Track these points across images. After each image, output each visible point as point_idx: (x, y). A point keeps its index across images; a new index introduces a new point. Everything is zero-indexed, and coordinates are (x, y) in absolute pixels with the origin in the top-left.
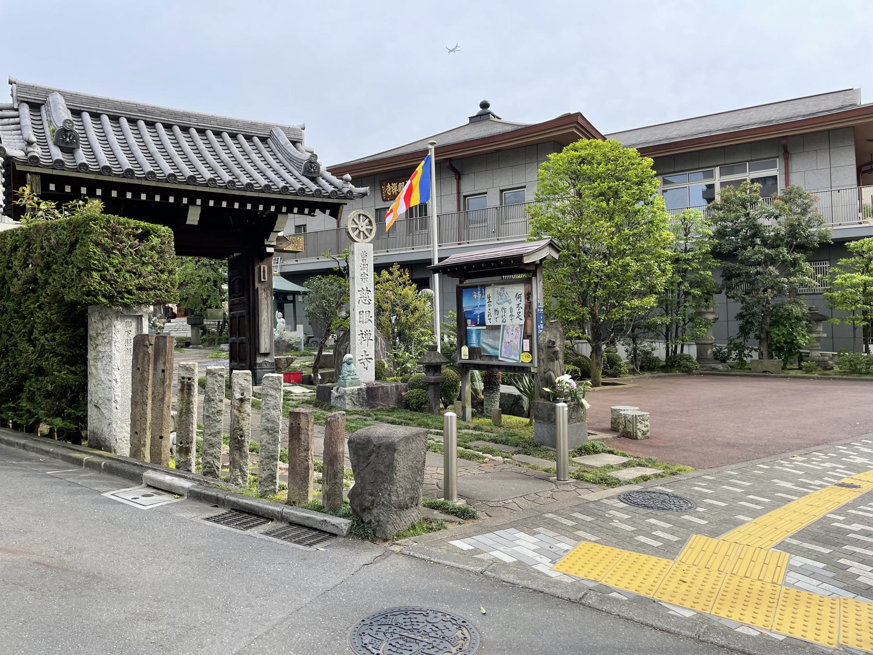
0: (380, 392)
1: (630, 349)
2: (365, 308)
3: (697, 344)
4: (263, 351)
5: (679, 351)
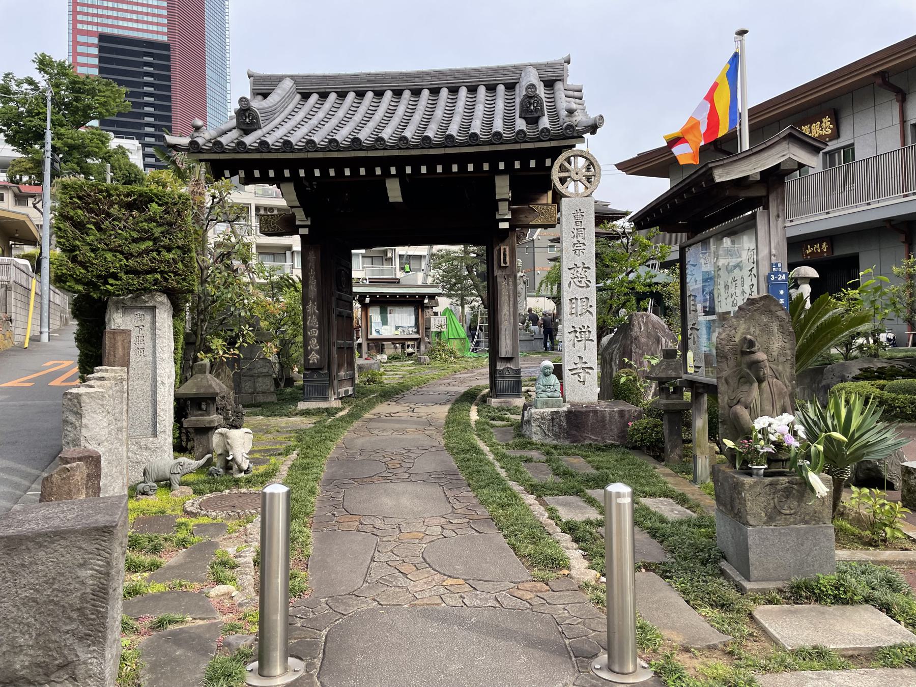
0: (591, 419)
2: (580, 293)
4: (503, 354)
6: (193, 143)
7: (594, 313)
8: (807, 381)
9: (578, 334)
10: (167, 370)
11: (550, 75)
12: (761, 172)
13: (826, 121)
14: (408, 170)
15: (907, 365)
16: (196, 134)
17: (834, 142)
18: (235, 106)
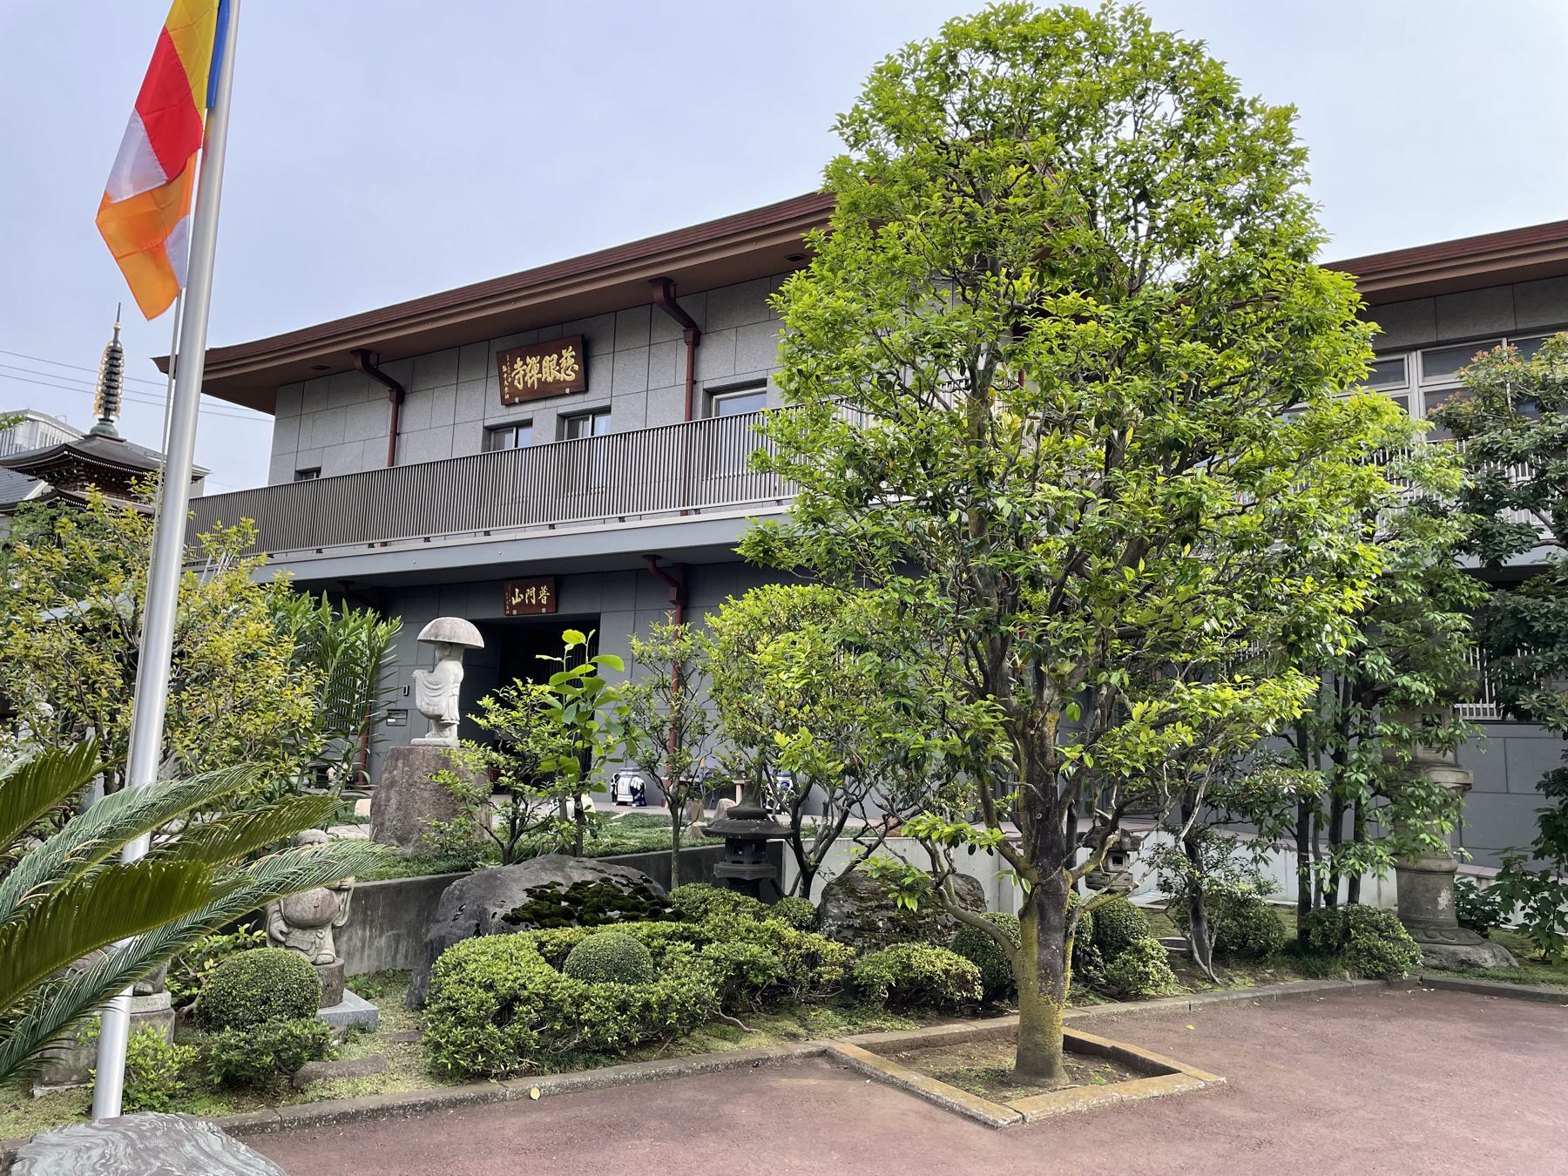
1: (1177, 882)
3: (1399, 869)
5: (1343, 895)
8: (410, 916)
13: (568, 354)
15: (634, 874)
17: (579, 398)
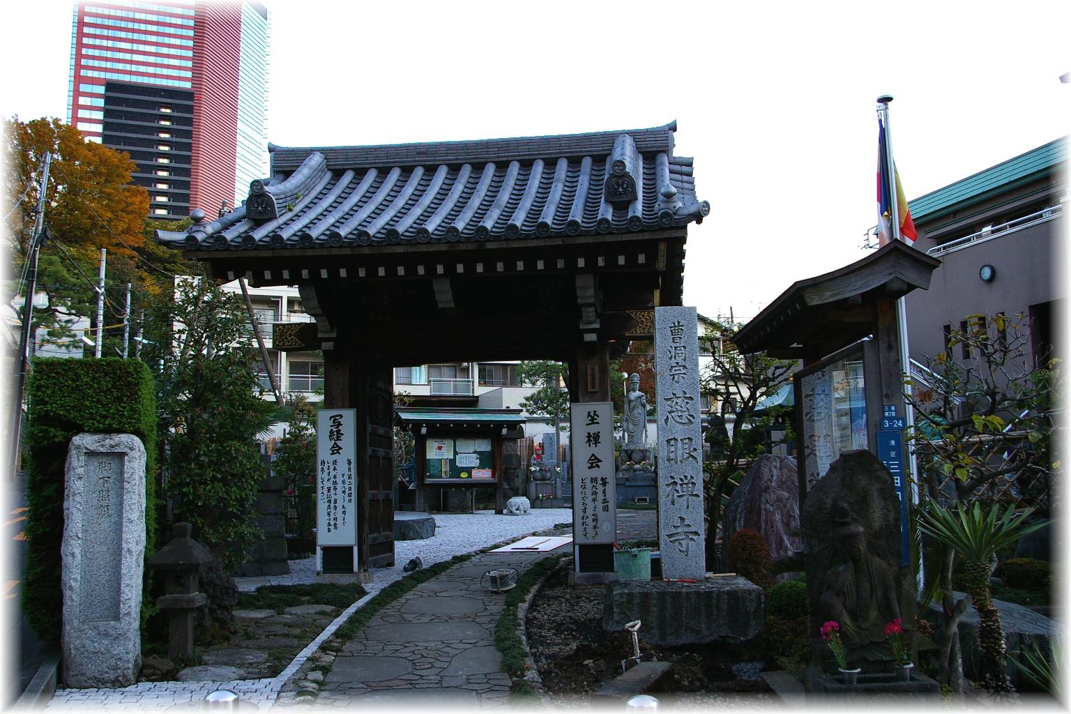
6: (191, 239)
7: (700, 459)
9: (678, 487)
10: (136, 535)
11: (651, 145)
12: (863, 295)
14: (460, 268)
16: (195, 228)
18: (241, 193)
